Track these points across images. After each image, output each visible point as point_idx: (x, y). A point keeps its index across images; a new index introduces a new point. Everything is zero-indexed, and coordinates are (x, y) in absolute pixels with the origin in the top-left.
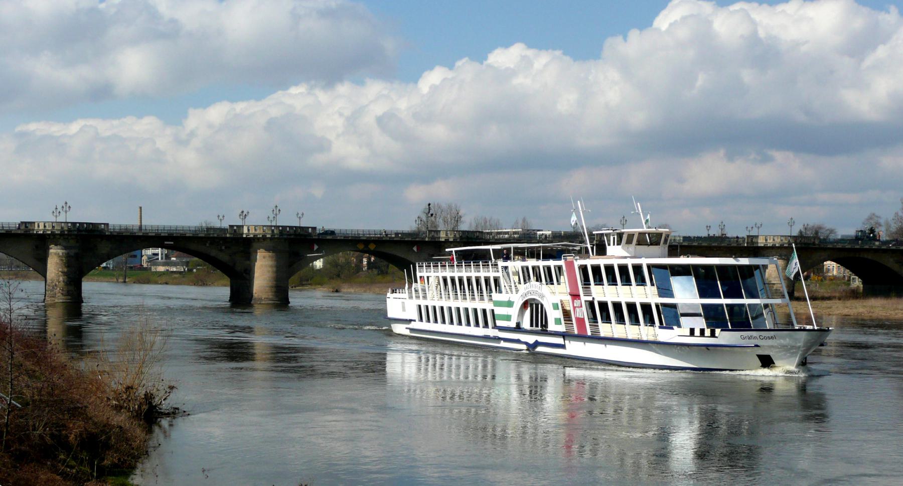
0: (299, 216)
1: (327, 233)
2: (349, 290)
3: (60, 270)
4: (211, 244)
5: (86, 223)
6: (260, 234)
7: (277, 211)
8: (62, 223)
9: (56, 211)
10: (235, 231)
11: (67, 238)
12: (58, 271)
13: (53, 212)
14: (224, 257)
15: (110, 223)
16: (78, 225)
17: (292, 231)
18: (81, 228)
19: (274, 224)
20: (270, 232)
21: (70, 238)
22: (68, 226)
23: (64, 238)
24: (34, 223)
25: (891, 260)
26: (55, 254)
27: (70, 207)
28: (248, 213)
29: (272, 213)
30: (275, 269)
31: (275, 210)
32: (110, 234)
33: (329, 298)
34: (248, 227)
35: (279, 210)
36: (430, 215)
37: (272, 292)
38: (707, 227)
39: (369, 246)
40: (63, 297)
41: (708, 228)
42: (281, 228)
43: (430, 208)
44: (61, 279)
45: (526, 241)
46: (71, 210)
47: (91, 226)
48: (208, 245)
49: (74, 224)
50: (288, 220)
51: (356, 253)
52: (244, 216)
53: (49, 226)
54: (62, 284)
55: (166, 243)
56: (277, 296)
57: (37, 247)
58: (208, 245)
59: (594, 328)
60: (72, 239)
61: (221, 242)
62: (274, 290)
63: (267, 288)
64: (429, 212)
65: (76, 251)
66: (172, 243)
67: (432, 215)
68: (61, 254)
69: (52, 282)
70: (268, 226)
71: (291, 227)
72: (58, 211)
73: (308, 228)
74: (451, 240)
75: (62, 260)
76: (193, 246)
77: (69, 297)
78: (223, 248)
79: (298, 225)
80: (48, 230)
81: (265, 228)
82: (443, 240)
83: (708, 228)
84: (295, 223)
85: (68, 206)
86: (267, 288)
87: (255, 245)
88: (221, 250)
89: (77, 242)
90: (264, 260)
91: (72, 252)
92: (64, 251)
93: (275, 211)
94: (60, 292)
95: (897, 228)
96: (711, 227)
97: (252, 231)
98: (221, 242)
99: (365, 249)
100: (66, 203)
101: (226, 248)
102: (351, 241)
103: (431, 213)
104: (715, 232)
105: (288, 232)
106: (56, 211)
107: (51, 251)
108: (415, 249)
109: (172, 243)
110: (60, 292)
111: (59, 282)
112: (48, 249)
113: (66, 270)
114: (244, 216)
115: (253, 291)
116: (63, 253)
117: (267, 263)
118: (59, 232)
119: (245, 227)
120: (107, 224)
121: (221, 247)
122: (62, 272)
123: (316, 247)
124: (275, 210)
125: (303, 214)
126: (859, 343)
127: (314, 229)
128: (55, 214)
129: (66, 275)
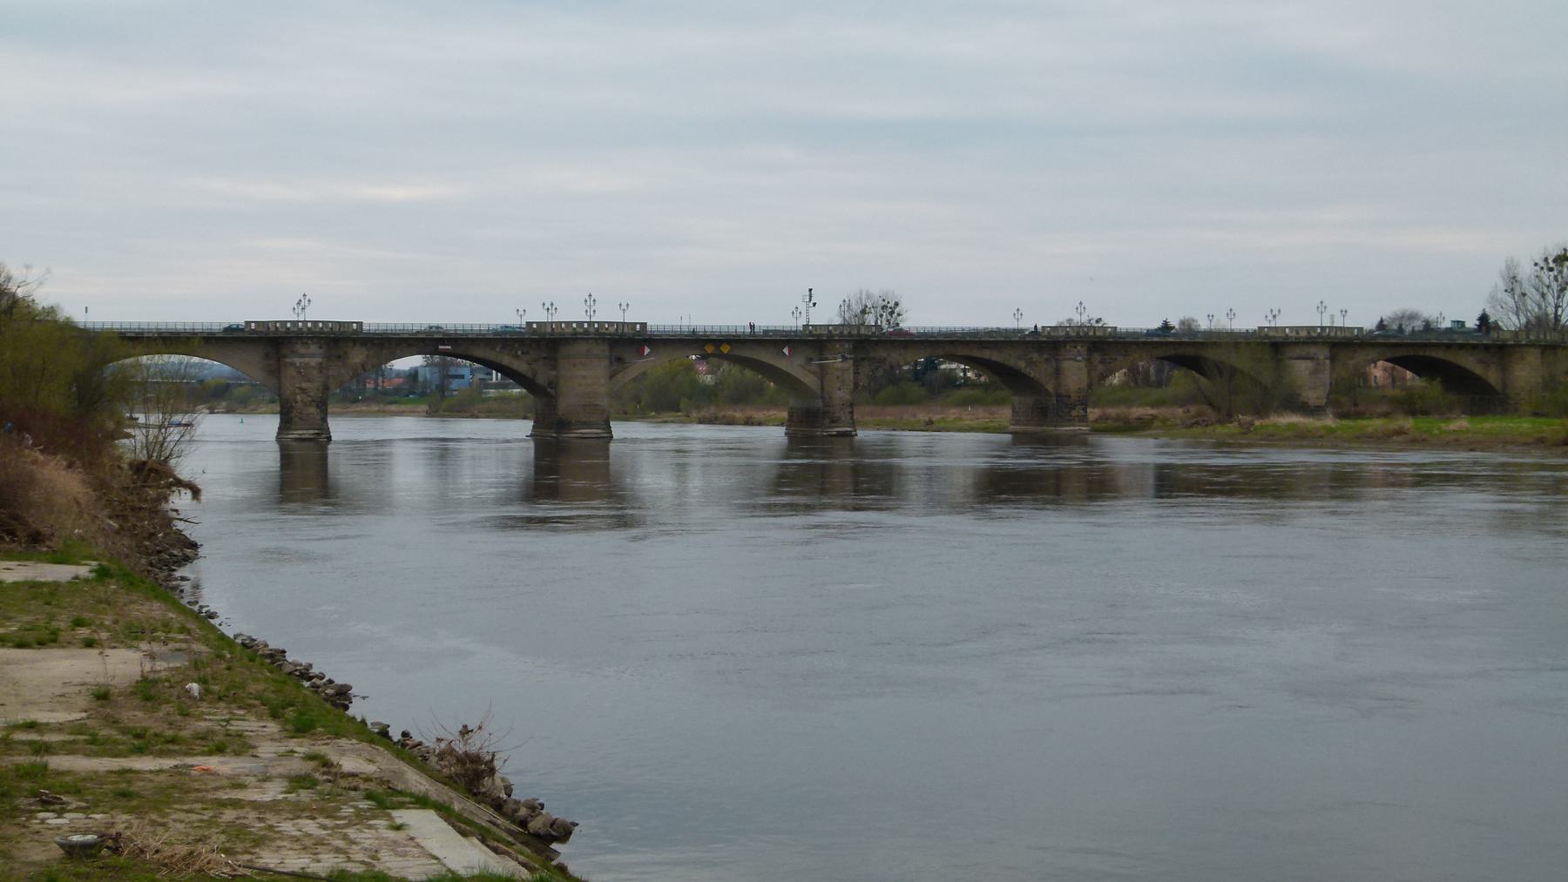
0: (546, 307)
2: (730, 413)
4: (503, 348)
5: (331, 322)
7: (590, 300)
13: (294, 309)
14: (520, 366)
15: (364, 322)
19: (1273, 325)
23: (303, 343)
25: (1471, 359)
33: (1220, 455)
35: (309, 301)
36: (811, 304)
38: (1342, 311)
39: (721, 348)
48: (498, 349)
51: (1178, 374)
55: (440, 347)
57: (267, 355)
60: (314, 343)
61: (516, 345)
64: (810, 300)
67: (814, 304)
71: (611, 324)
72: (592, 310)
73: (287, 322)
78: (519, 353)
79: (1016, 327)
84: (617, 317)
85: (307, 298)
88: (517, 357)
96: (527, 312)
100: (590, 295)
101: (523, 353)
103: (812, 302)
104: (538, 316)
108: (786, 351)
109: (450, 347)
114: (1344, 313)
121: (516, 352)
123: (647, 350)
125: (628, 305)
126: (666, 422)
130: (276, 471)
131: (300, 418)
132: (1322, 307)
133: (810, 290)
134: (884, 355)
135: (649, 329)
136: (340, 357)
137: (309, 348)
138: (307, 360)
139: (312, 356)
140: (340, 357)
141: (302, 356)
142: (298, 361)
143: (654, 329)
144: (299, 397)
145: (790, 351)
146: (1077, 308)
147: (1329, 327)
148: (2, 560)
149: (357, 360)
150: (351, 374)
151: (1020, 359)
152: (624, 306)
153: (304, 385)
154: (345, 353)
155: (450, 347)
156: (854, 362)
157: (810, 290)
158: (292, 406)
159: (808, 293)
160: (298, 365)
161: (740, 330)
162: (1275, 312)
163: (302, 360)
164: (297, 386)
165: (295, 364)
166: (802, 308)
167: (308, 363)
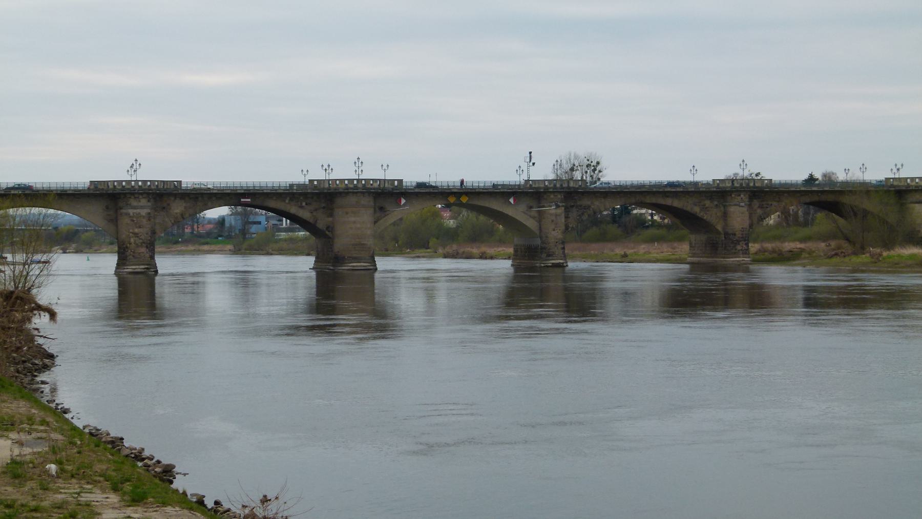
1: (420, 185)
4: (291, 200)
5: (373, 180)
7: (863, 168)
9: (863, 167)
11: (138, 198)
14: (305, 214)
16: (149, 183)
18: (153, 187)
22: (114, 186)
27: (362, 163)
29: (354, 165)
35: (140, 165)
36: (531, 164)
38: (845, 170)
41: (847, 171)
46: (903, 167)
48: (287, 201)
55: (242, 200)
58: (287, 201)
59: (651, 298)
64: (530, 161)
65: (149, 211)
66: (249, 200)
76: (272, 204)
78: (304, 204)
83: (847, 171)
88: (301, 207)
89: (149, 201)
93: (742, 166)
98: (301, 198)
99: (458, 202)
101: (306, 204)
102: (228, 194)
103: (532, 161)
104: (318, 174)
105: (917, 183)
106: (863, 167)
108: (512, 200)
109: (249, 200)
121: (301, 204)
123: (403, 201)
127: (400, 181)
128: (130, 173)
131: (133, 256)
133: (530, 153)
135: (404, 184)
136: (164, 208)
137: (140, 201)
138: (138, 211)
139: (142, 207)
140: (164, 208)
141: (135, 208)
142: (131, 211)
144: (132, 240)
145: (514, 201)
149: (178, 211)
150: (173, 222)
151: (696, 205)
152: (385, 167)
153: (136, 230)
154: (169, 205)
156: (565, 209)
157: (530, 153)
158: (127, 247)
160: (131, 214)
163: (135, 211)
164: (131, 231)
165: (129, 214)
166: (524, 167)
167: (139, 213)
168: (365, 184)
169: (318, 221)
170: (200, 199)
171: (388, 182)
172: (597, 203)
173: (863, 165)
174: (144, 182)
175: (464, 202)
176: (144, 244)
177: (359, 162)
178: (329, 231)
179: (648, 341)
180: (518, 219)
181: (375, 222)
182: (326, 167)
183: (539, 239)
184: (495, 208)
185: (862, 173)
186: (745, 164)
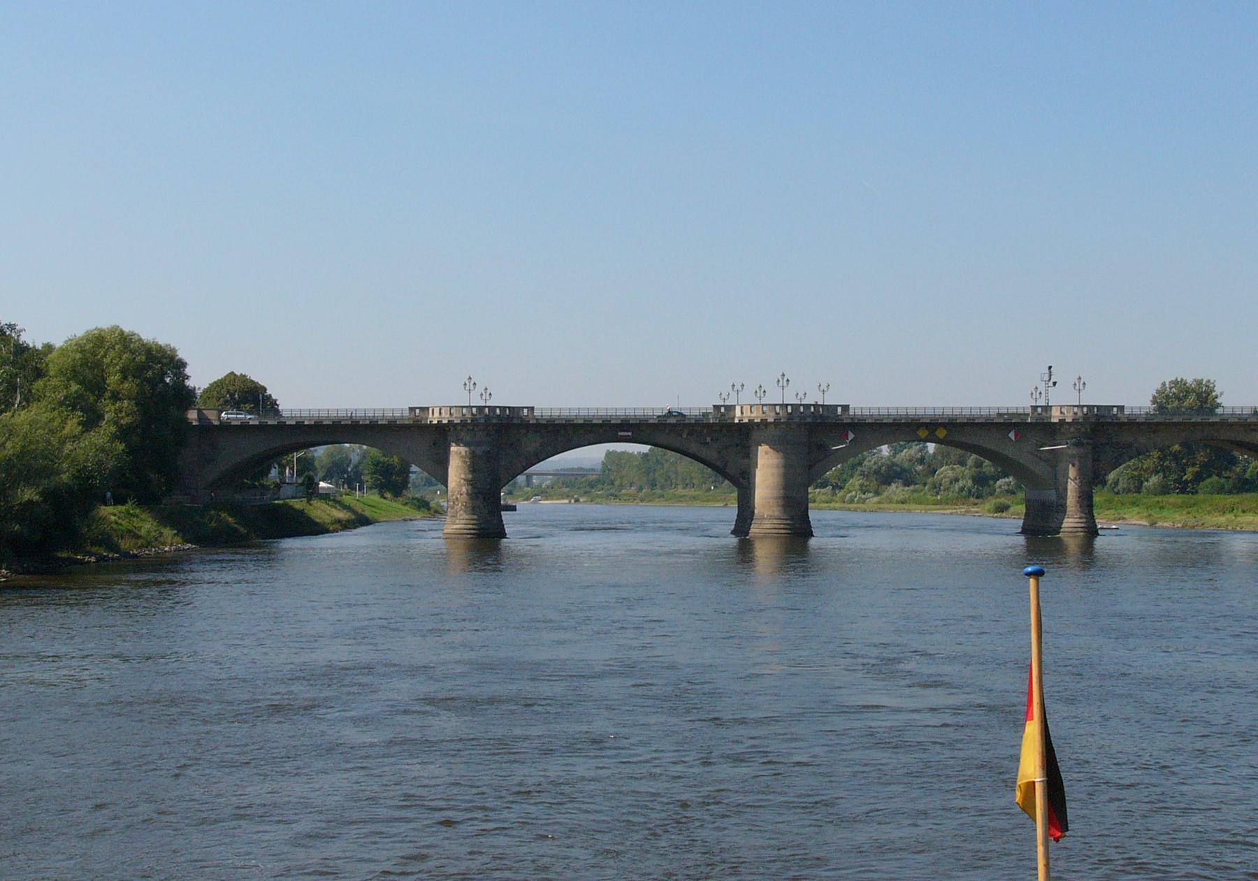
3: (463, 476)
6: (757, 417)
7: (784, 381)
8: (463, 407)
9: (1079, 382)
10: (723, 415)
12: (460, 478)
15: (1126, 406)
17: (807, 412)
20: (773, 414)
21: (476, 429)
22: (472, 414)
24: (428, 408)
26: (456, 453)
28: (1221, 394)
30: (782, 470)
31: (781, 380)
32: (535, 422)
34: (742, 408)
36: (1051, 384)
37: (778, 506)
39: (937, 433)
40: (467, 517)
42: (789, 408)
43: (1050, 372)
44: (464, 489)
45: (586, 443)
47: (508, 411)
48: (685, 436)
49: (1090, 407)
50: (505, 397)
52: (738, 389)
53: (446, 413)
54: (464, 498)
55: (620, 434)
56: (785, 512)
58: (685, 436)
62: (781, 502)
63: (771, 501)
64: (1050, 380)
67: (1055, 384)
68: (463, 454)
69: (453, 495)
70: (769, 405)
73: (1094, 406)
74: (1069, 420)
75: (465, 462)
77: (475, 517)
78: (708, 440)
80: (444, 418)
81: (765, 408)
82: (1056, 420)
86: (771, 501)
87: (755, 435)
90: (766, 456)
91: (479, 451)
92: (467, 449)
94: (461, 509)
95: (458, 466)
96: (807, 396)
97: (747, 413)
103: (1052, 381)
106: (1079, 382)
107: (452, 449)
108: (1012, 435)
109: (630, 434)
110: (461, 509)
111: (461, 495)
112: (449, 446)
113: (470, 476)
115: (754, 501)
116: (466, 452)
117: (771, 461)
118: (459, 422)
119: (737, 407)
120: (532, 409)
122: (465, 480)
123: (851, 436)
124: (781, 380)
127: (1121, 408)
129: (471, 485)
130: (1022, 545)
132: (470, 385)
134: (1131, 439)
135: (851, 412)
143: (858, 412)
145: (1016, 435)
146: (482, 394)
147: (813, 405)
148: (4, 605)
154: (518, 440)
155: (630, 434)
156: (1094, 448)
157: (1050, 368)
159: (1047, 371)
161: (397, 414)
162: (824, 387)
166: (1042, 388)
168: (791, 414)
169: (728, 464)
170: (562, 432)
171: (828, 409)
172: (1142, 440)
173: (470, 378)
174: (503, 409)
175: (941, 438)
176: (479, 495)
177: (784, 381)
178: (744, 478)
179: (851, 729)
180: (449, 474)
181: (810, 467)
182: (824, 387)
183: (1053, 492)
184: (989, 446)
185: (468, 392)
186: (472, 383)
